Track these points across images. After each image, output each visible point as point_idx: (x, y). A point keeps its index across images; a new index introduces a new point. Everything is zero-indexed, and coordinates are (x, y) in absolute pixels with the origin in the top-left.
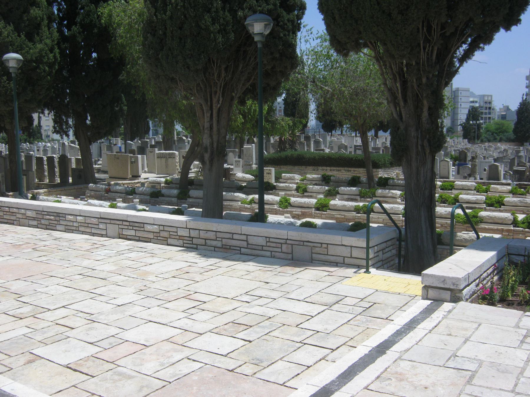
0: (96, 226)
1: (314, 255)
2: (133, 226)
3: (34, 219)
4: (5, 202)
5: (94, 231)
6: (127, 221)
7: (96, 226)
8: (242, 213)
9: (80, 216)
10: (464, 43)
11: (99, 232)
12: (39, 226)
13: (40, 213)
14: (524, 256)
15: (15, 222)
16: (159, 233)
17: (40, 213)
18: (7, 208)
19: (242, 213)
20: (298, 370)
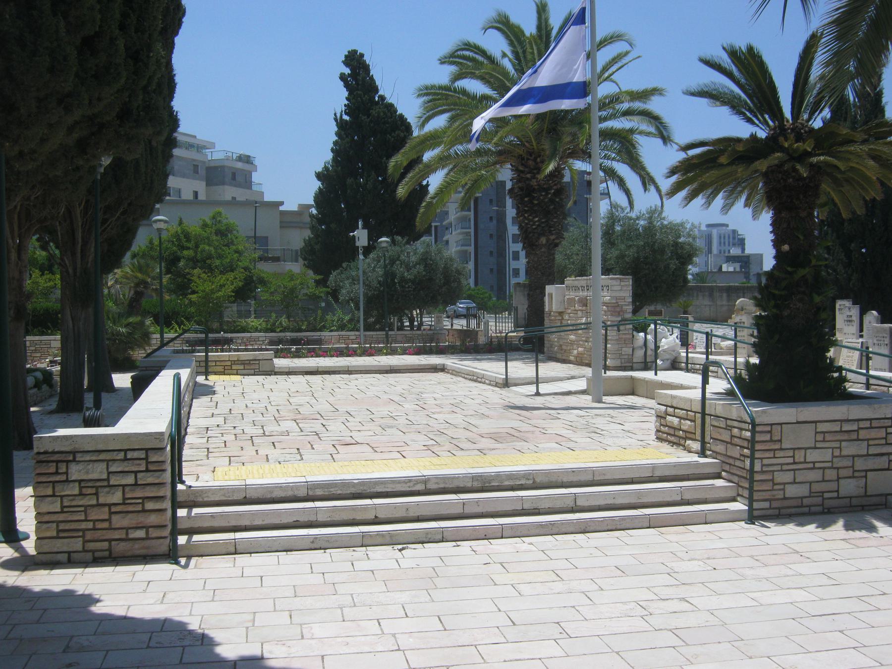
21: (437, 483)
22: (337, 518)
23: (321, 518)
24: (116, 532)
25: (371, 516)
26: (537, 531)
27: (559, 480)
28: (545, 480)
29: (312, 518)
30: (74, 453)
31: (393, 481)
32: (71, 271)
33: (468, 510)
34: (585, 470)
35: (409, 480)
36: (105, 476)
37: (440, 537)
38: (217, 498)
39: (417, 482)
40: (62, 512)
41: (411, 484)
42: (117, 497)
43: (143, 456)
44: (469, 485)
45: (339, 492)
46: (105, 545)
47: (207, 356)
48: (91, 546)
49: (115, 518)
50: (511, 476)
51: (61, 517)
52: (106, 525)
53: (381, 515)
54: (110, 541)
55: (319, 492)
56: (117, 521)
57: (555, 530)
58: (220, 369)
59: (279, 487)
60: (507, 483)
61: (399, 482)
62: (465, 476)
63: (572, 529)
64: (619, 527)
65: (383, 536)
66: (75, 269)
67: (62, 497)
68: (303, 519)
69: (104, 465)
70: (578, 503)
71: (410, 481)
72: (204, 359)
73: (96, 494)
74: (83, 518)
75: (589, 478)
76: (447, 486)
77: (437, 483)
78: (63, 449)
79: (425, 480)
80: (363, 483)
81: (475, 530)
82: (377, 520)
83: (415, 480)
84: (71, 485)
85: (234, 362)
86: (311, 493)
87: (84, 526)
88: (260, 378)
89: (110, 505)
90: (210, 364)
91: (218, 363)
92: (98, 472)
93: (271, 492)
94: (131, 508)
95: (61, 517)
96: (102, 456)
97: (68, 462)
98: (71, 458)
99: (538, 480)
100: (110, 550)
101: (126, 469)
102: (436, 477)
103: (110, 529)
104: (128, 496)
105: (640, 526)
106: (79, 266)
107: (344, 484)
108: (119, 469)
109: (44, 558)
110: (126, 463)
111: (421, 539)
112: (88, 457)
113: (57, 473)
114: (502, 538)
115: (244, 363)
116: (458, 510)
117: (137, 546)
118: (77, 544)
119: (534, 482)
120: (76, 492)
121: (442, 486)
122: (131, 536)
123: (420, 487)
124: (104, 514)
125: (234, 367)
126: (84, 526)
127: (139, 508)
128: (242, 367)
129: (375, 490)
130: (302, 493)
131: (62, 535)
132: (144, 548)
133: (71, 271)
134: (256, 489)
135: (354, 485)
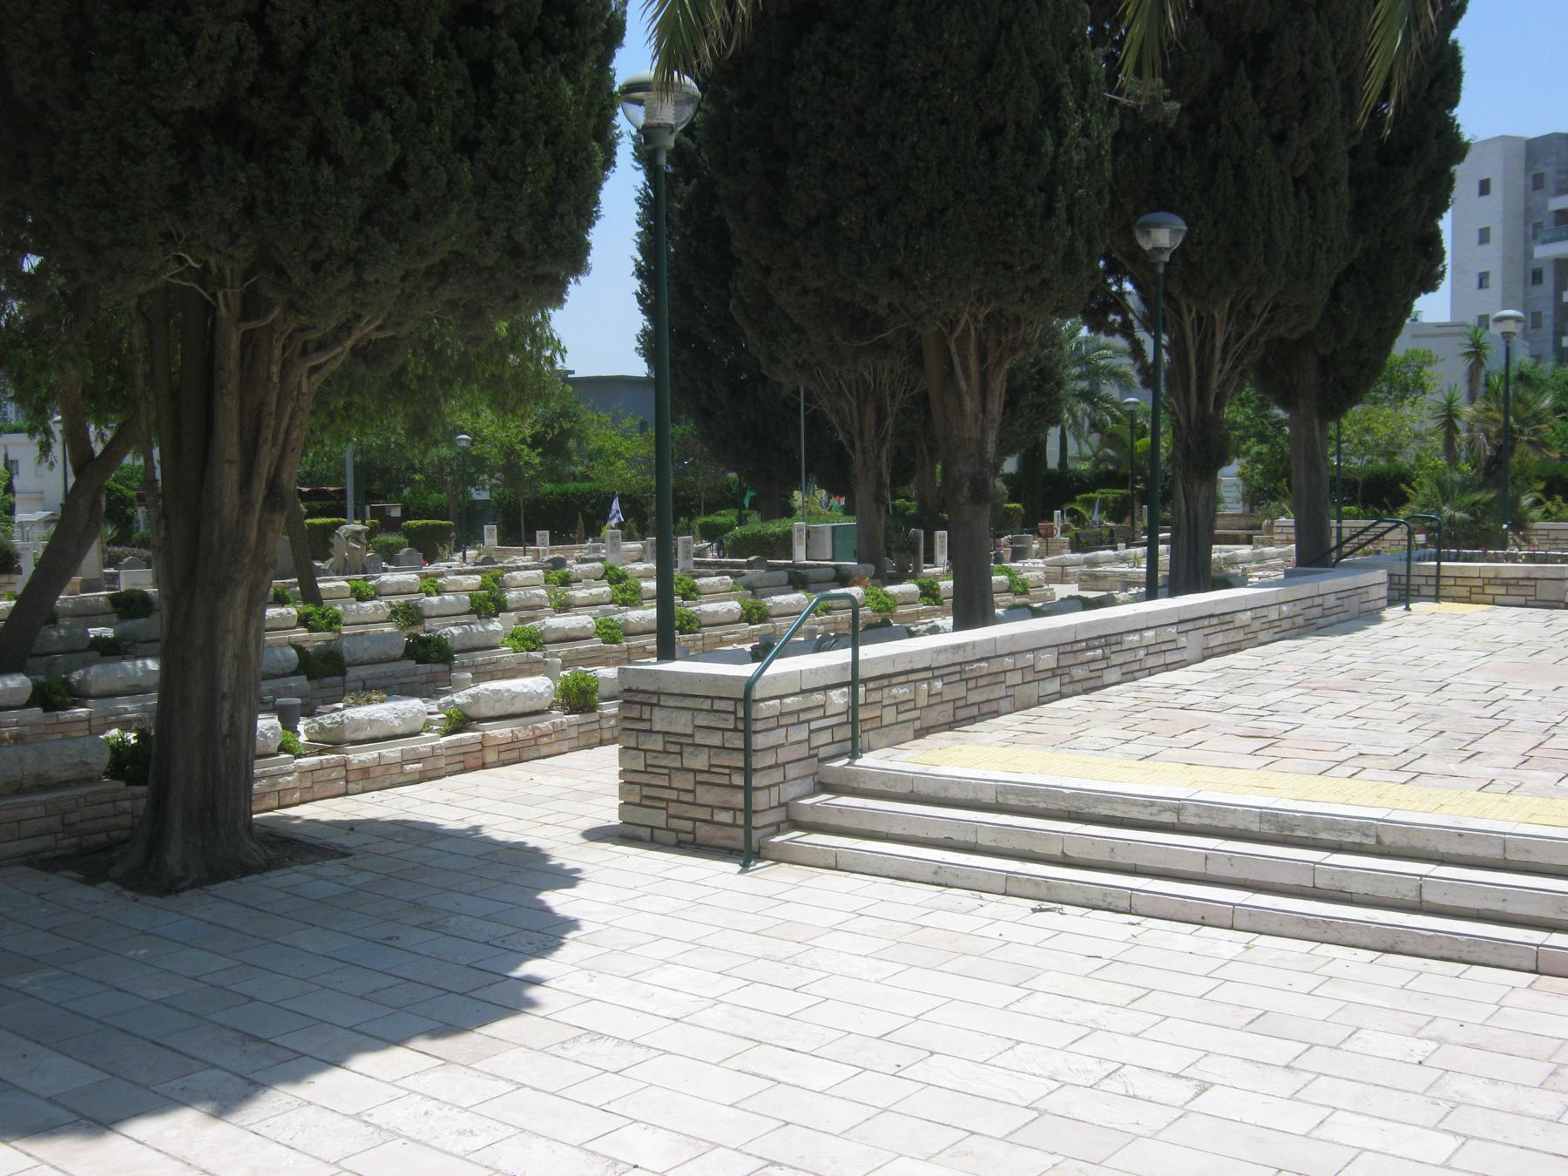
0: (1173, 646)
1: (740, 744)
2: (712, 711)
3: (1053, 673)
4: (974, 644)
5: (1170, 658)
6: (1212, 616)
7: (1173, 646)
8: (158, 475)
9: (1148, 628)
10: (1167, 265)
11: (1179, 658)
12: (1065, 689)
13: (1068, 648)
14: (1408, 575)
15: (1005, 705)
16: (692, 736)
17: (1068, 648)
18: (984, 664)
19: (158, 475)
20: (1323, 1132)
21: (1197, 815)
22: (1006, 844)
23: (984, 840)
24: (701, 809)
25: (1054, 850)
26: (1298, 930)
27: (1431, 847)
28: (1402, 842)
29: (971, 838)
30: (658, 694)
31: (1129, 800)
32: (1182, 420)
33: (1215, 870)
34: (1485, 836)
35: (1150, 803)
36: (689, 731)
37: (1125, 904)
38: (877, 786)
39: (1165, 809)
40: (645, 772)
41: (1154, 810)
42: (700, 761)
43: (731, 709)
44: (1255, 827)
45: (1042, 805)
46: (688, 825)
47: (1438, 567)
48: (675, 823)
49: (700, 789)
50: (1333, 823)
51: (644, 778)
52: (689, 798)
53: (1072, 852)
54: (694, 820)
55: (1012, 800)
56: (704, 795)
57: (1332, 936)
58: (1463, 592)
59: (958, 782)
60: (1324, 836)
61: (1135, 803)
62: (1247, 810)
63: (1366, 940)
64: (1465, 956)
65: (1037, 884)
66: (1188, 417)
67: (645, 751)
68: (958, 836)
69: (688, 715)
70: (1426, 897)
71: (1152, 804)
72: (1434, 572)
73: (681, 754)
74: (666, 784)
75: (1495, 852)
76: (1215, 823)
77: (1197, 815)
78: (646, 688)
79: (1178, 807)
80: (1078, 795)
81: (1185, 904)
82: (1067, 860)
83: (1161, 805)
84: (654, 737)
85: (1489, 581)
86: (1000, 799)
87: (667, 794)
88: (1541, 614)
89: (695, 771)
90: (1443, 582)
91: (1459, 582)
92: (682, 724)
93: (946, 789)
94: (717, 780)
95: (644, 778)
96: (688, 703)
97: (652, 705)
98: (654, 700)
99: (1387, 840)
100: (693, 832)
101: (713, 725)
102: (1198, 804)
103: (694, 804)
104: (714, 762)
105: (1513, 963)
106: (1193, 412)
107: (1051, 793)
108: (705, 723)
109: (630, 830)
110: (711, 716)
111: (1095, 902)
112: (672, 702)
113: (641, 719)
114: (1232, 928)
115: (1506, 583)
116: (1196, 867)
117: (720, 834)
118: (659, 818)
119: (1379, 842)
120: (659, 747)
121: (1206, 821)
122: (716, 818)
123: (1168, 818)
124: (686, 782)
125: (1489, 590)
126: (667, 794)
127: (725, 780)
128: (1502, 590)
129: (1096, 811)
130: (988, 797)
131: (646, 802)
132: (729, 838)
133: (1182, 420)
134: (925, 780)
135: (1065, 797)
